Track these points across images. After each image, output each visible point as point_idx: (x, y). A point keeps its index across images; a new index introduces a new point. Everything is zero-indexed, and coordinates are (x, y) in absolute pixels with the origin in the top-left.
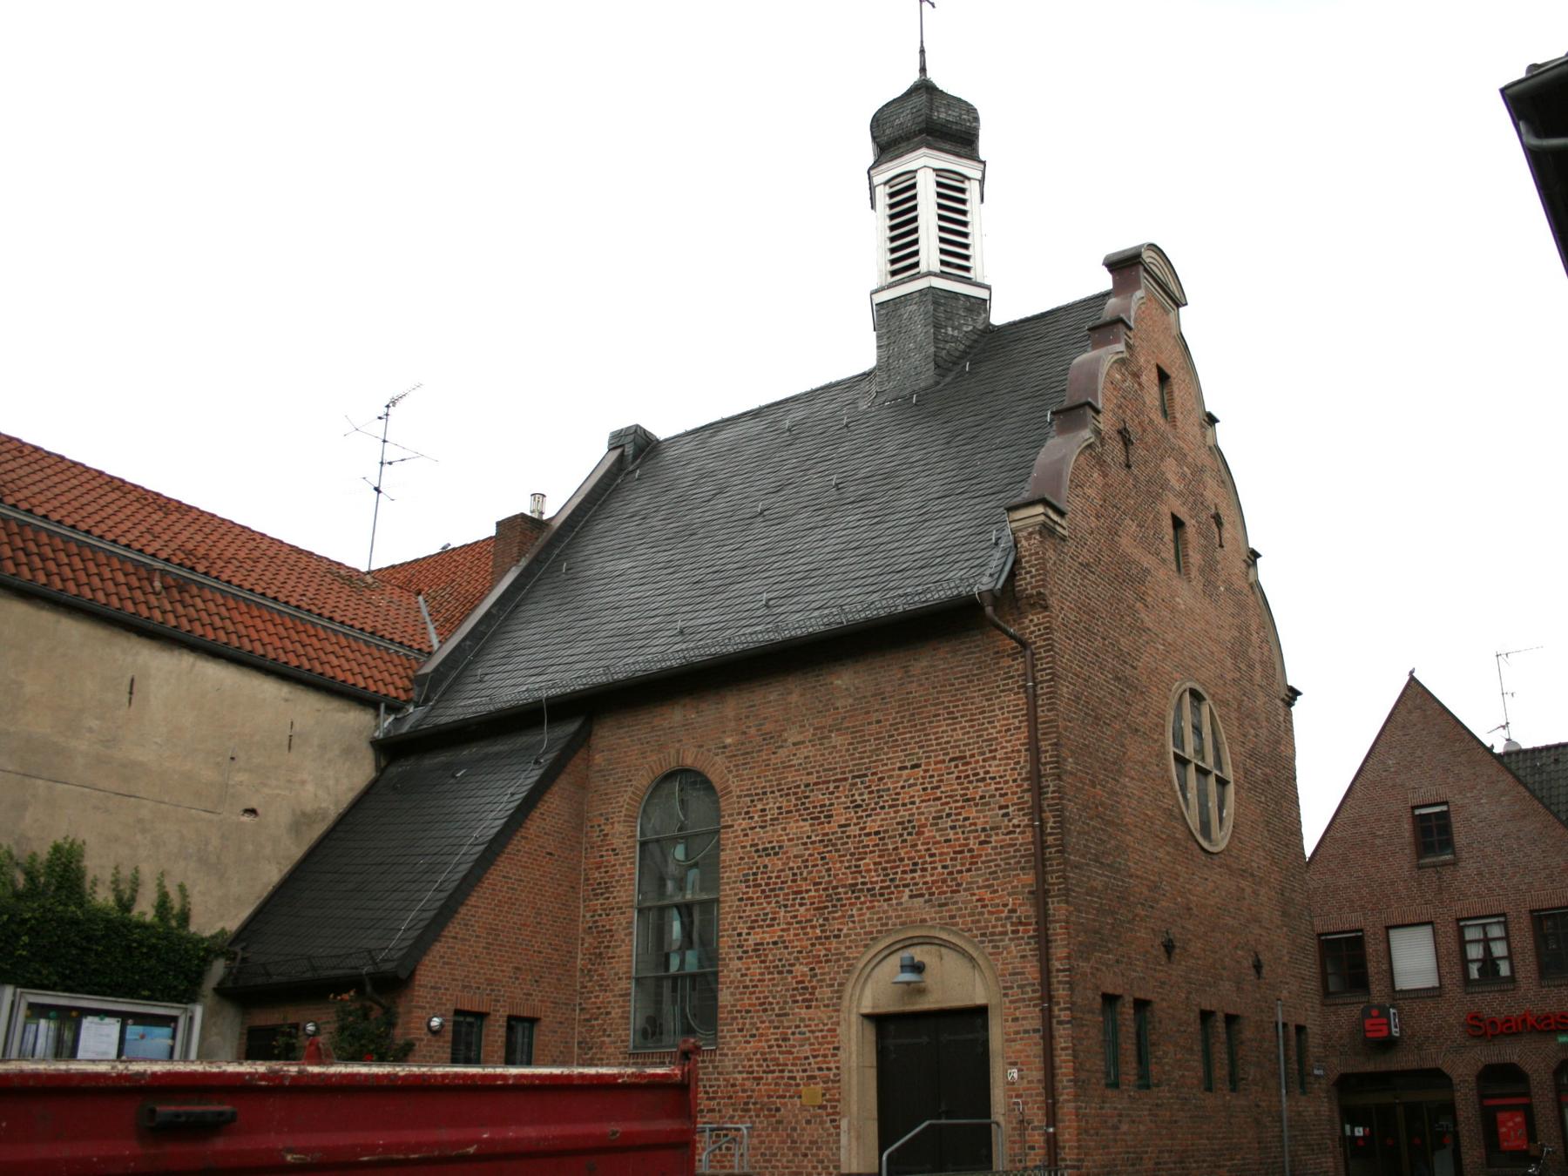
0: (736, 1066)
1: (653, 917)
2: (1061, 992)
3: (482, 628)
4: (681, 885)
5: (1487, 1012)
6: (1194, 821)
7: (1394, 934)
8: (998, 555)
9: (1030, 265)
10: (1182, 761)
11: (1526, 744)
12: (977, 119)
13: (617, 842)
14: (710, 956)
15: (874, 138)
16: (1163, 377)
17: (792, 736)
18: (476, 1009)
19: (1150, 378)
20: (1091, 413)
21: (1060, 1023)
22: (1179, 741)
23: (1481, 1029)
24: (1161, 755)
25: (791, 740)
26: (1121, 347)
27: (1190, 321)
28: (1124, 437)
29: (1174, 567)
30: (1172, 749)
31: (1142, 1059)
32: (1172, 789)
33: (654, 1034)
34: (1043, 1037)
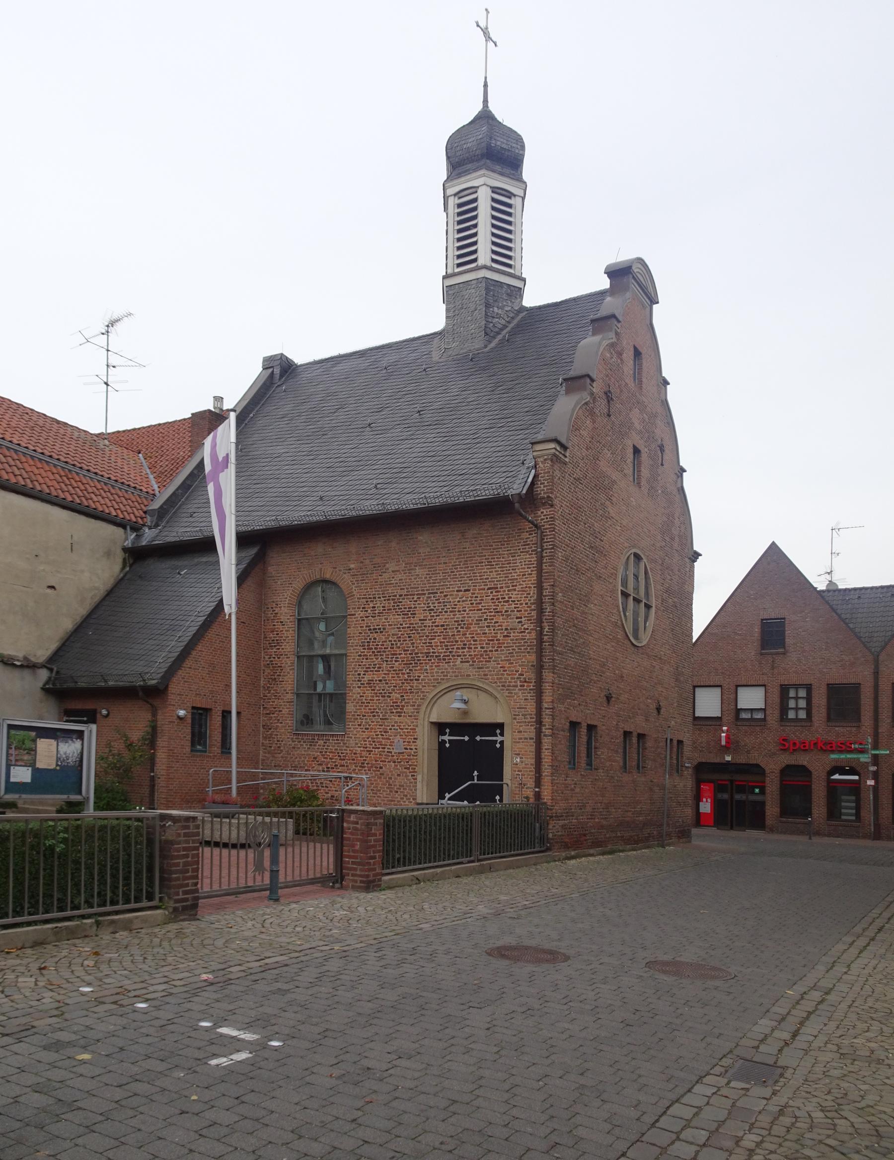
0: (357, 744)
1: (306, 660)
2: (547, 720)
3: (189, 482)
4: (324, 644)
5: (792, 737)
6: (629, 629)
7: (740, 690)
8: (524, 471)
9: (555, 270)
10: (625, 595)
11: (841, 586)
12: (523, 147)
13: (283, 618)
14: (341, 683)
15: (448, 158)
16: (637, 353)
17: (391, 566)
18: (203, 706)
19: (628, 355)
20: (588, 381)
21: (545, 735)
22: (625, 583)
23: (786, 745)
24: (613, 591)
25: (390, 570)
26: (612, 335)
27: (660, 315)
28: (608, 397)
29: (631, 479)
30: (620, 588)
31: (589, 755)
32: (618, 610)
33: (308, 723)
34: (535, 742)
